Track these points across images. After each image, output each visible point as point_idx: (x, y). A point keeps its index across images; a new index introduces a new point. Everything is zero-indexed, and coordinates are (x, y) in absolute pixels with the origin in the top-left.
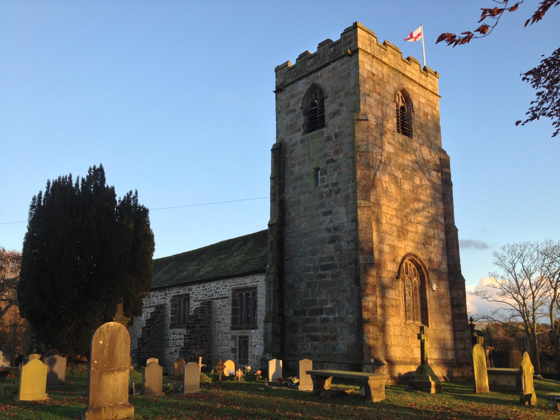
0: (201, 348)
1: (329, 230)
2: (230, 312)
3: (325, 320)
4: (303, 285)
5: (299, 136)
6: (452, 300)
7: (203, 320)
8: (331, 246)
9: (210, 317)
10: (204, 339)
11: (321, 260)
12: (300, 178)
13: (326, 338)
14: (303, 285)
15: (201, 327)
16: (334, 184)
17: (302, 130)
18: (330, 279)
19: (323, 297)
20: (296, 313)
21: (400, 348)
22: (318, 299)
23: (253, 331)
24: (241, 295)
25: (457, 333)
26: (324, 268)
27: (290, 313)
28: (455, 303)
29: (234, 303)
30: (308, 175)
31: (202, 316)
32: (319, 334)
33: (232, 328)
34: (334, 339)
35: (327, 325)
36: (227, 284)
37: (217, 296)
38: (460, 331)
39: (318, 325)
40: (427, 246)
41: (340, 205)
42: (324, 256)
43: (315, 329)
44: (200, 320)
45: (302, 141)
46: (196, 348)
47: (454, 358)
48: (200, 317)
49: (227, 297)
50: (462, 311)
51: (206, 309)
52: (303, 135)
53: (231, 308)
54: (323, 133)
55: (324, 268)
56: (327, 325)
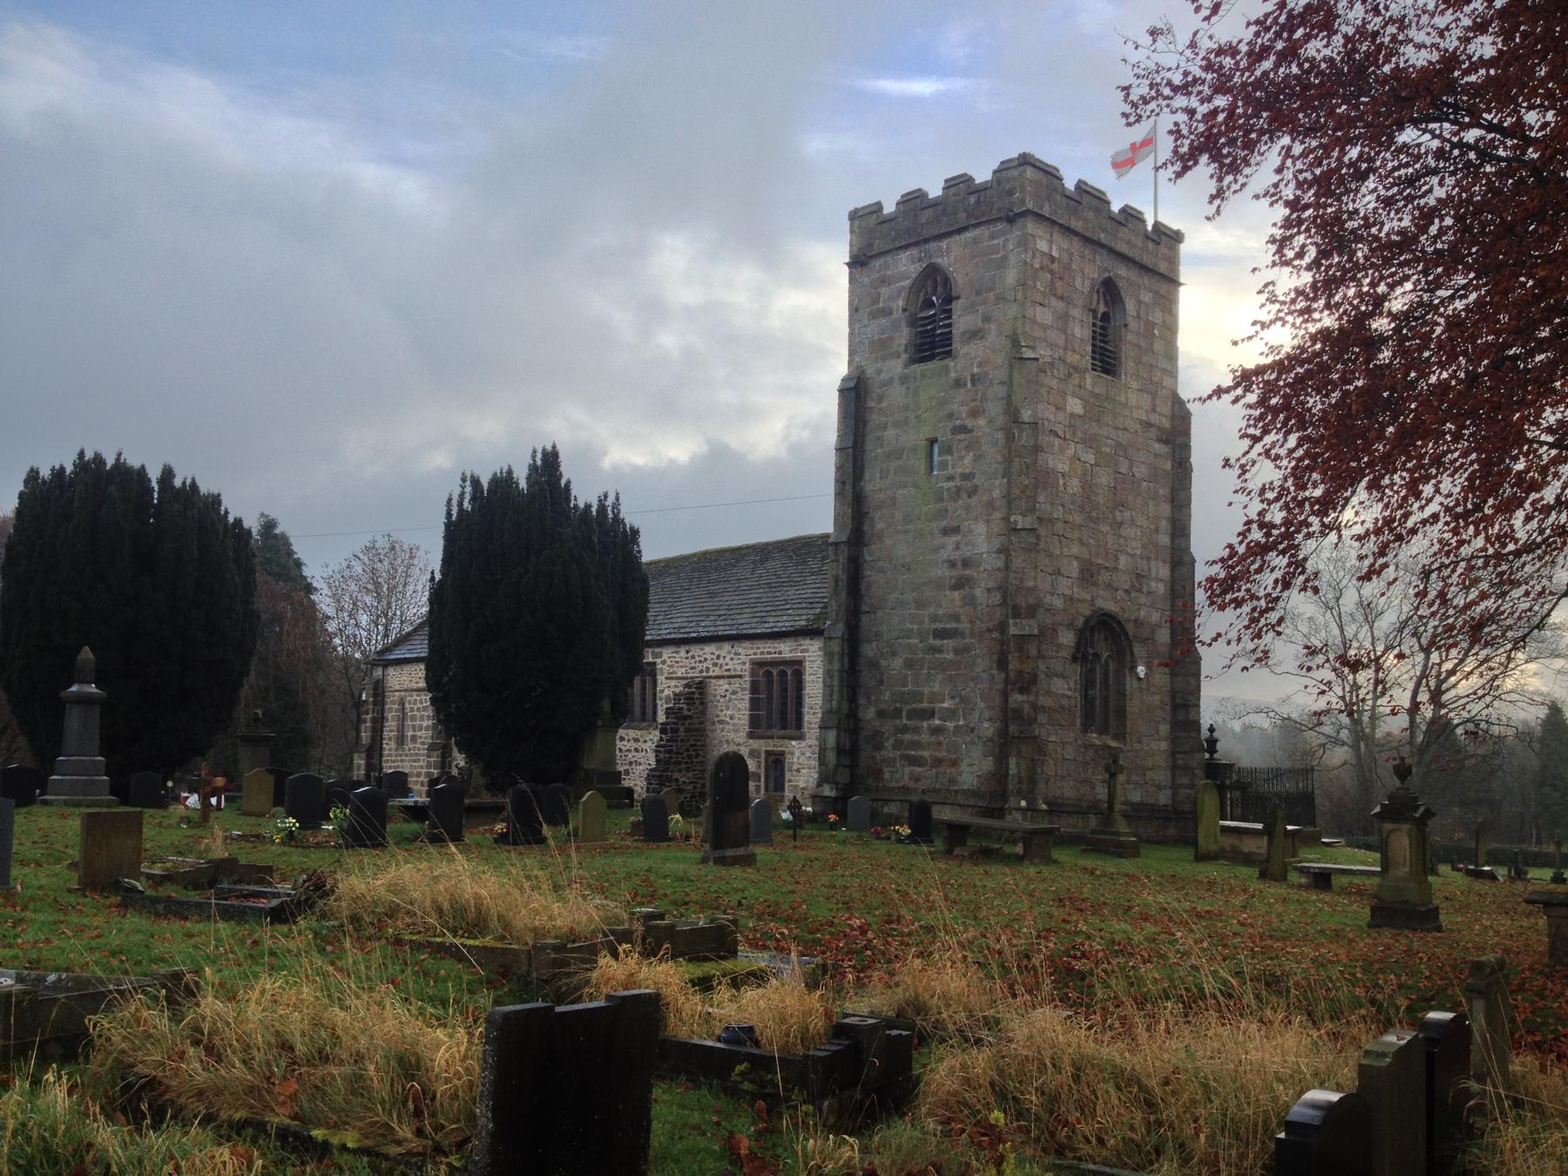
0: (688, 769)
1: (952, 564)
2: (746, 704)
3: (937, 731)
4: (897, 663)
5: (896, 367)
6: (1173, 694)
7: (691, 717)
8: (956, 594)
9: (703, 713)
10: (693, 753)
11: (935, 618)
12: (897, 454)
13: (938, 762)
14: (897, 663)
15: (687, 730)
16: (967, 477)
17: (905, 356)
18: (950, 656)
19: (937, 687)
20: (881, 714)
21: (1072, 783)
22: (926, 690)
23: (794, 743)
24: (769, 673)
25: (1179, 756)
26: (941, 634)
27: (869, 714)
28: (1178, 701)
29: (755, 688)
30: (914, 450)
31: (689, 710)
32: (926, 754)
33: (751, 735)
34: (954, 763)
35: (941, 738)
36: (740, 650)
37: (717, 672)
38: (1185, 752)
39: (925, 737)
40: (1133, 595)
41: (976, 519)
42: (941, 612)
43: (917, 745)
44: (686, 718)
45: (904, 379)
46: (680, 771)
47: (1170, 802)
48: (686, 712)
49: (740, 676)
50: (1191, 717)
51: (696, 696)
52: (906, 366)
53: (747, 697)
54: (947, 370)
55: (941, 634)
56: (941, 738)
